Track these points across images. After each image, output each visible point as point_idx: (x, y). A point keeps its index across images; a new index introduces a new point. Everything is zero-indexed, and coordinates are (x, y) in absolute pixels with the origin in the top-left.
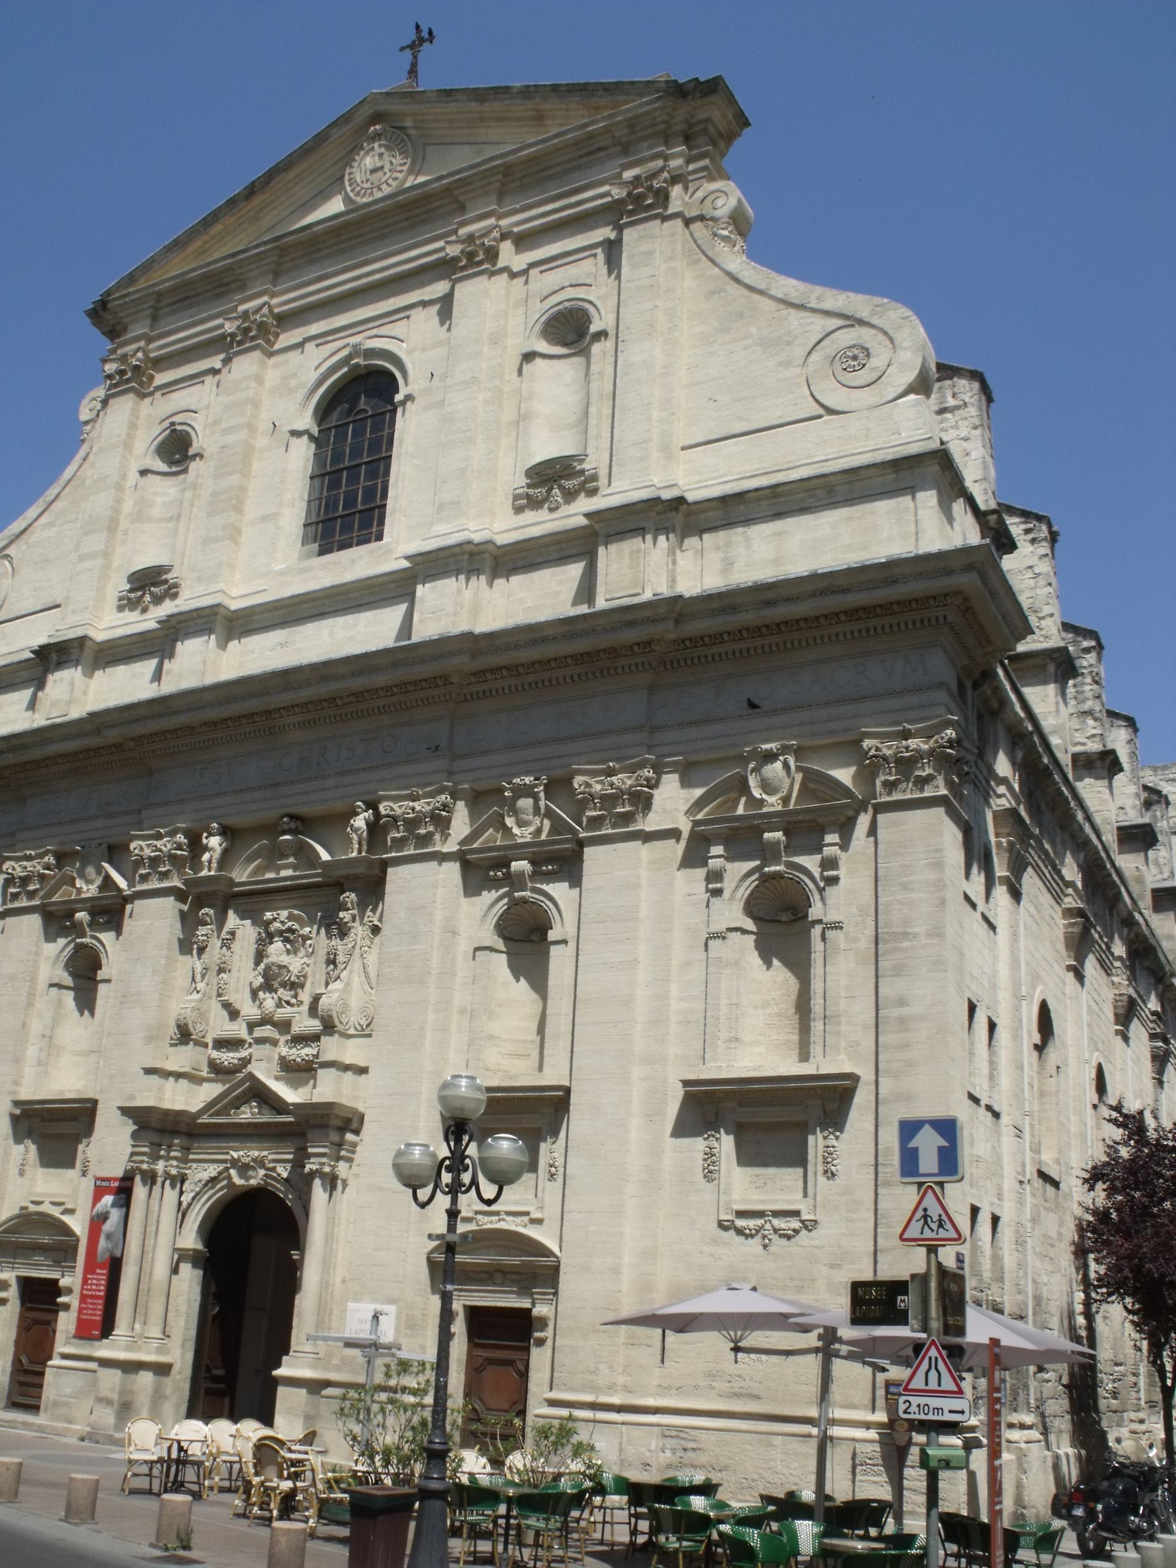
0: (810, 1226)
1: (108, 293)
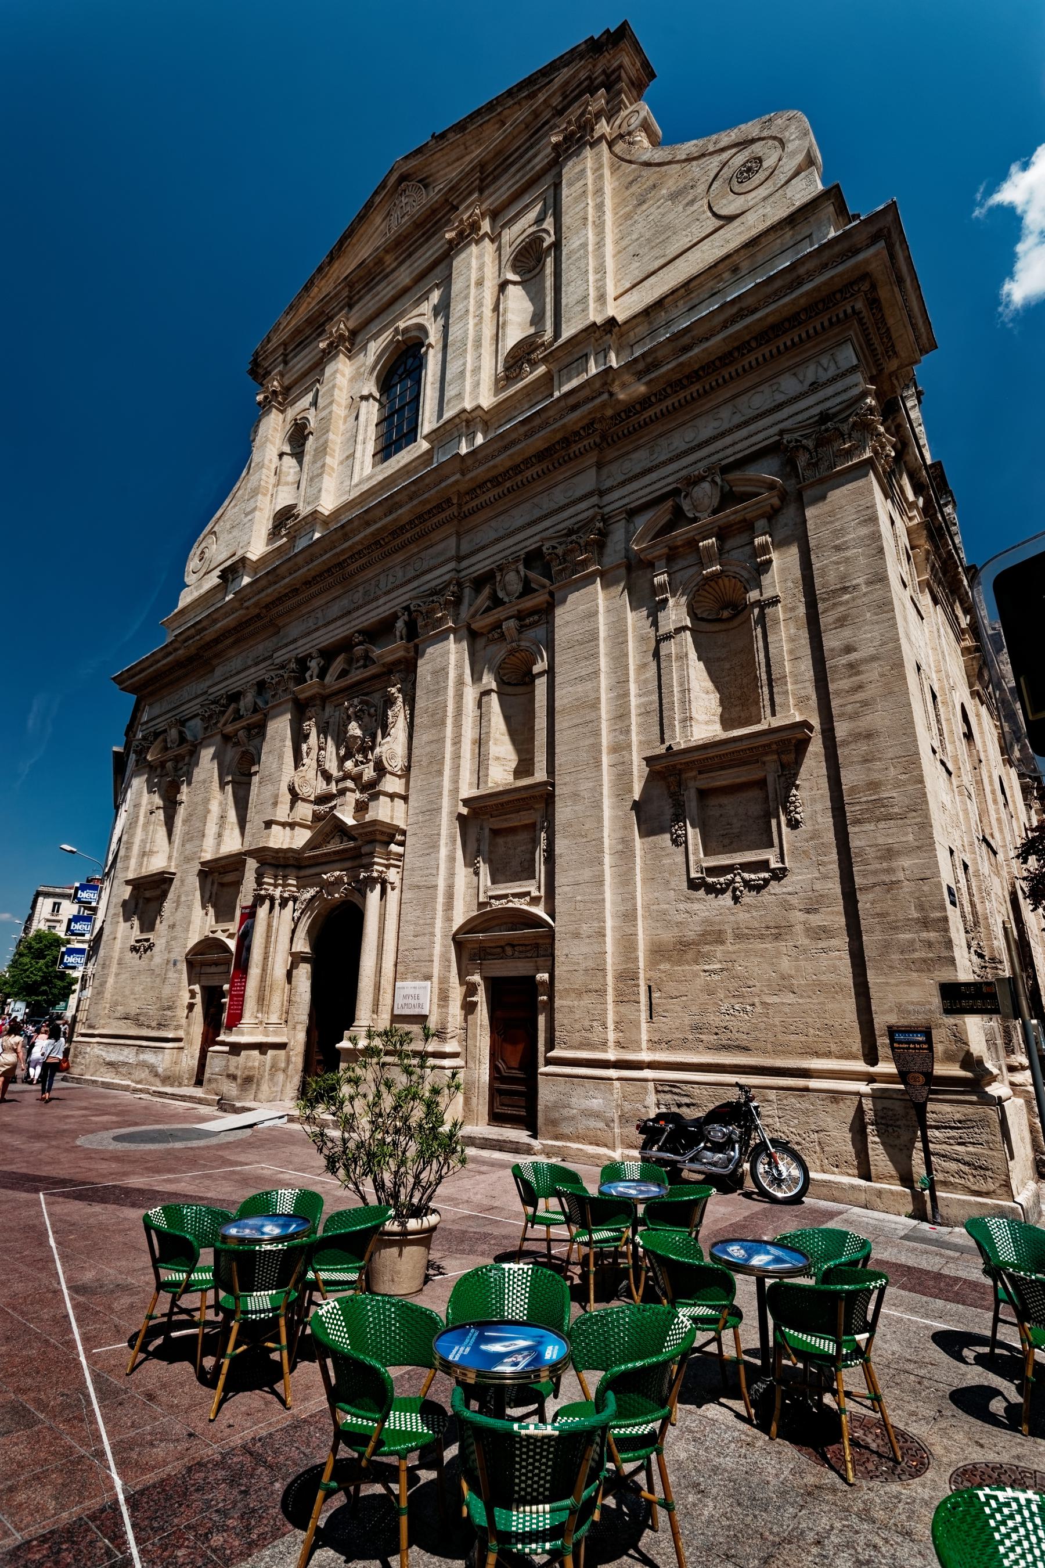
0: (779, 875)
1: (257, 353)
